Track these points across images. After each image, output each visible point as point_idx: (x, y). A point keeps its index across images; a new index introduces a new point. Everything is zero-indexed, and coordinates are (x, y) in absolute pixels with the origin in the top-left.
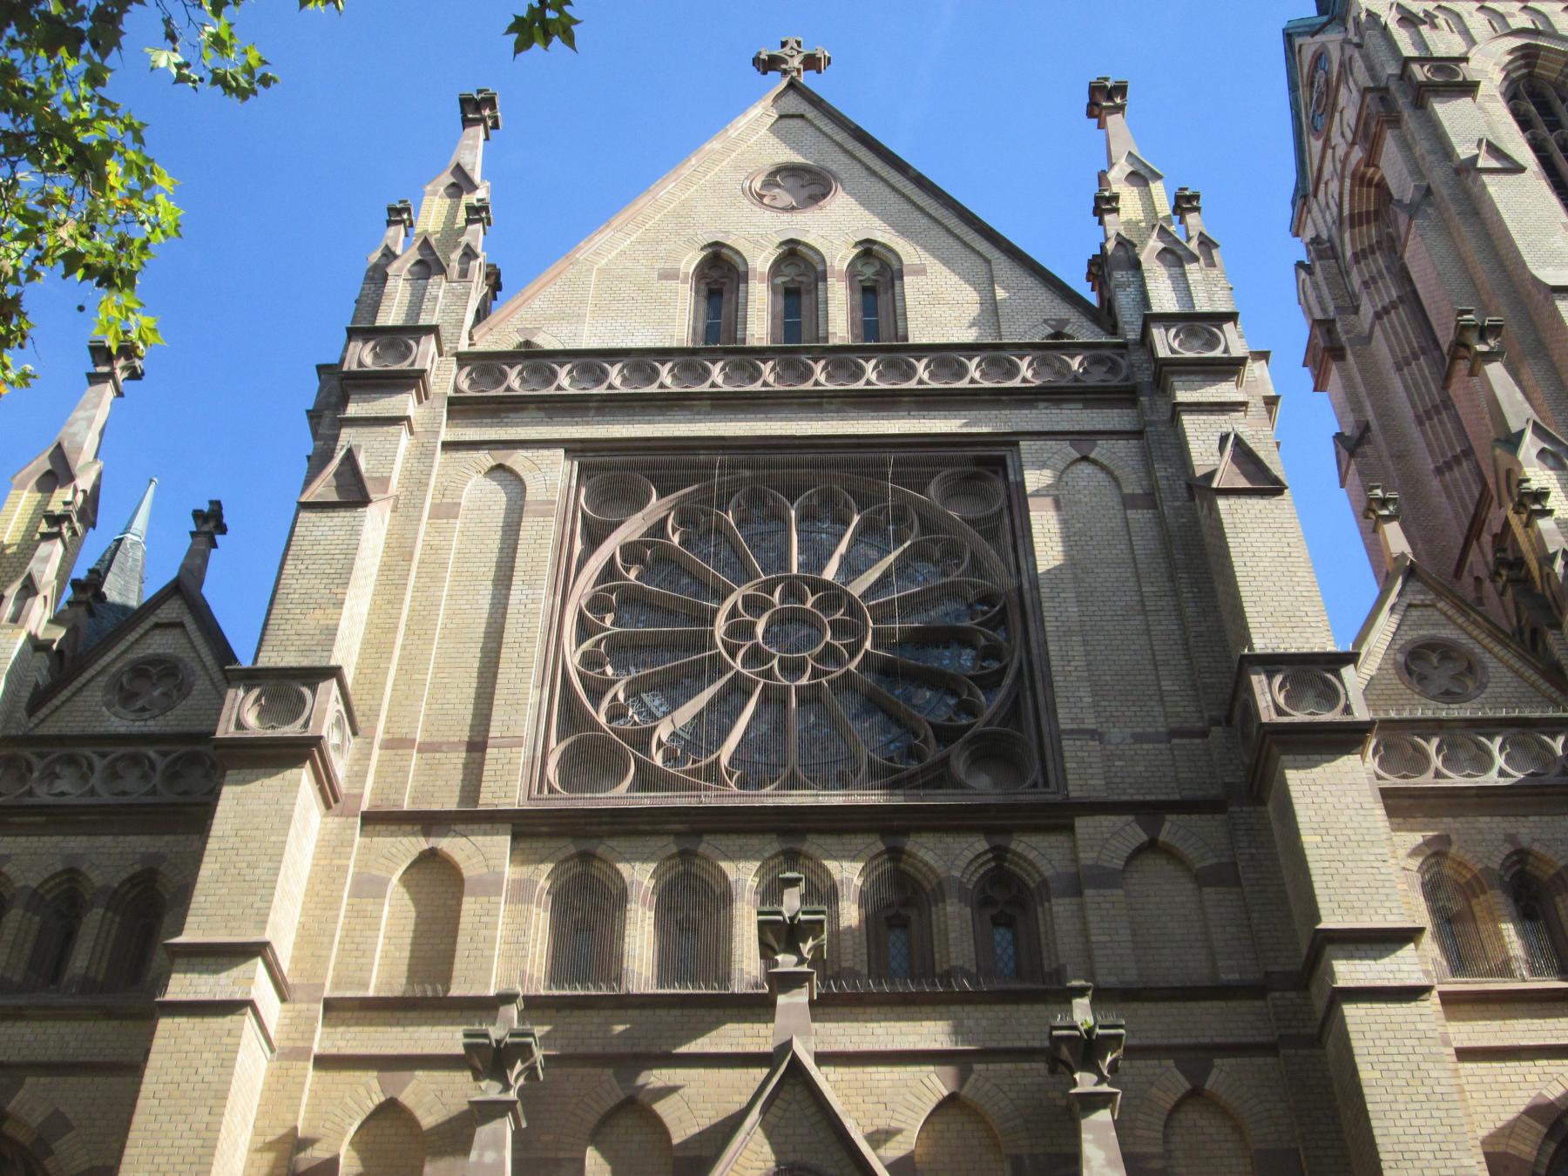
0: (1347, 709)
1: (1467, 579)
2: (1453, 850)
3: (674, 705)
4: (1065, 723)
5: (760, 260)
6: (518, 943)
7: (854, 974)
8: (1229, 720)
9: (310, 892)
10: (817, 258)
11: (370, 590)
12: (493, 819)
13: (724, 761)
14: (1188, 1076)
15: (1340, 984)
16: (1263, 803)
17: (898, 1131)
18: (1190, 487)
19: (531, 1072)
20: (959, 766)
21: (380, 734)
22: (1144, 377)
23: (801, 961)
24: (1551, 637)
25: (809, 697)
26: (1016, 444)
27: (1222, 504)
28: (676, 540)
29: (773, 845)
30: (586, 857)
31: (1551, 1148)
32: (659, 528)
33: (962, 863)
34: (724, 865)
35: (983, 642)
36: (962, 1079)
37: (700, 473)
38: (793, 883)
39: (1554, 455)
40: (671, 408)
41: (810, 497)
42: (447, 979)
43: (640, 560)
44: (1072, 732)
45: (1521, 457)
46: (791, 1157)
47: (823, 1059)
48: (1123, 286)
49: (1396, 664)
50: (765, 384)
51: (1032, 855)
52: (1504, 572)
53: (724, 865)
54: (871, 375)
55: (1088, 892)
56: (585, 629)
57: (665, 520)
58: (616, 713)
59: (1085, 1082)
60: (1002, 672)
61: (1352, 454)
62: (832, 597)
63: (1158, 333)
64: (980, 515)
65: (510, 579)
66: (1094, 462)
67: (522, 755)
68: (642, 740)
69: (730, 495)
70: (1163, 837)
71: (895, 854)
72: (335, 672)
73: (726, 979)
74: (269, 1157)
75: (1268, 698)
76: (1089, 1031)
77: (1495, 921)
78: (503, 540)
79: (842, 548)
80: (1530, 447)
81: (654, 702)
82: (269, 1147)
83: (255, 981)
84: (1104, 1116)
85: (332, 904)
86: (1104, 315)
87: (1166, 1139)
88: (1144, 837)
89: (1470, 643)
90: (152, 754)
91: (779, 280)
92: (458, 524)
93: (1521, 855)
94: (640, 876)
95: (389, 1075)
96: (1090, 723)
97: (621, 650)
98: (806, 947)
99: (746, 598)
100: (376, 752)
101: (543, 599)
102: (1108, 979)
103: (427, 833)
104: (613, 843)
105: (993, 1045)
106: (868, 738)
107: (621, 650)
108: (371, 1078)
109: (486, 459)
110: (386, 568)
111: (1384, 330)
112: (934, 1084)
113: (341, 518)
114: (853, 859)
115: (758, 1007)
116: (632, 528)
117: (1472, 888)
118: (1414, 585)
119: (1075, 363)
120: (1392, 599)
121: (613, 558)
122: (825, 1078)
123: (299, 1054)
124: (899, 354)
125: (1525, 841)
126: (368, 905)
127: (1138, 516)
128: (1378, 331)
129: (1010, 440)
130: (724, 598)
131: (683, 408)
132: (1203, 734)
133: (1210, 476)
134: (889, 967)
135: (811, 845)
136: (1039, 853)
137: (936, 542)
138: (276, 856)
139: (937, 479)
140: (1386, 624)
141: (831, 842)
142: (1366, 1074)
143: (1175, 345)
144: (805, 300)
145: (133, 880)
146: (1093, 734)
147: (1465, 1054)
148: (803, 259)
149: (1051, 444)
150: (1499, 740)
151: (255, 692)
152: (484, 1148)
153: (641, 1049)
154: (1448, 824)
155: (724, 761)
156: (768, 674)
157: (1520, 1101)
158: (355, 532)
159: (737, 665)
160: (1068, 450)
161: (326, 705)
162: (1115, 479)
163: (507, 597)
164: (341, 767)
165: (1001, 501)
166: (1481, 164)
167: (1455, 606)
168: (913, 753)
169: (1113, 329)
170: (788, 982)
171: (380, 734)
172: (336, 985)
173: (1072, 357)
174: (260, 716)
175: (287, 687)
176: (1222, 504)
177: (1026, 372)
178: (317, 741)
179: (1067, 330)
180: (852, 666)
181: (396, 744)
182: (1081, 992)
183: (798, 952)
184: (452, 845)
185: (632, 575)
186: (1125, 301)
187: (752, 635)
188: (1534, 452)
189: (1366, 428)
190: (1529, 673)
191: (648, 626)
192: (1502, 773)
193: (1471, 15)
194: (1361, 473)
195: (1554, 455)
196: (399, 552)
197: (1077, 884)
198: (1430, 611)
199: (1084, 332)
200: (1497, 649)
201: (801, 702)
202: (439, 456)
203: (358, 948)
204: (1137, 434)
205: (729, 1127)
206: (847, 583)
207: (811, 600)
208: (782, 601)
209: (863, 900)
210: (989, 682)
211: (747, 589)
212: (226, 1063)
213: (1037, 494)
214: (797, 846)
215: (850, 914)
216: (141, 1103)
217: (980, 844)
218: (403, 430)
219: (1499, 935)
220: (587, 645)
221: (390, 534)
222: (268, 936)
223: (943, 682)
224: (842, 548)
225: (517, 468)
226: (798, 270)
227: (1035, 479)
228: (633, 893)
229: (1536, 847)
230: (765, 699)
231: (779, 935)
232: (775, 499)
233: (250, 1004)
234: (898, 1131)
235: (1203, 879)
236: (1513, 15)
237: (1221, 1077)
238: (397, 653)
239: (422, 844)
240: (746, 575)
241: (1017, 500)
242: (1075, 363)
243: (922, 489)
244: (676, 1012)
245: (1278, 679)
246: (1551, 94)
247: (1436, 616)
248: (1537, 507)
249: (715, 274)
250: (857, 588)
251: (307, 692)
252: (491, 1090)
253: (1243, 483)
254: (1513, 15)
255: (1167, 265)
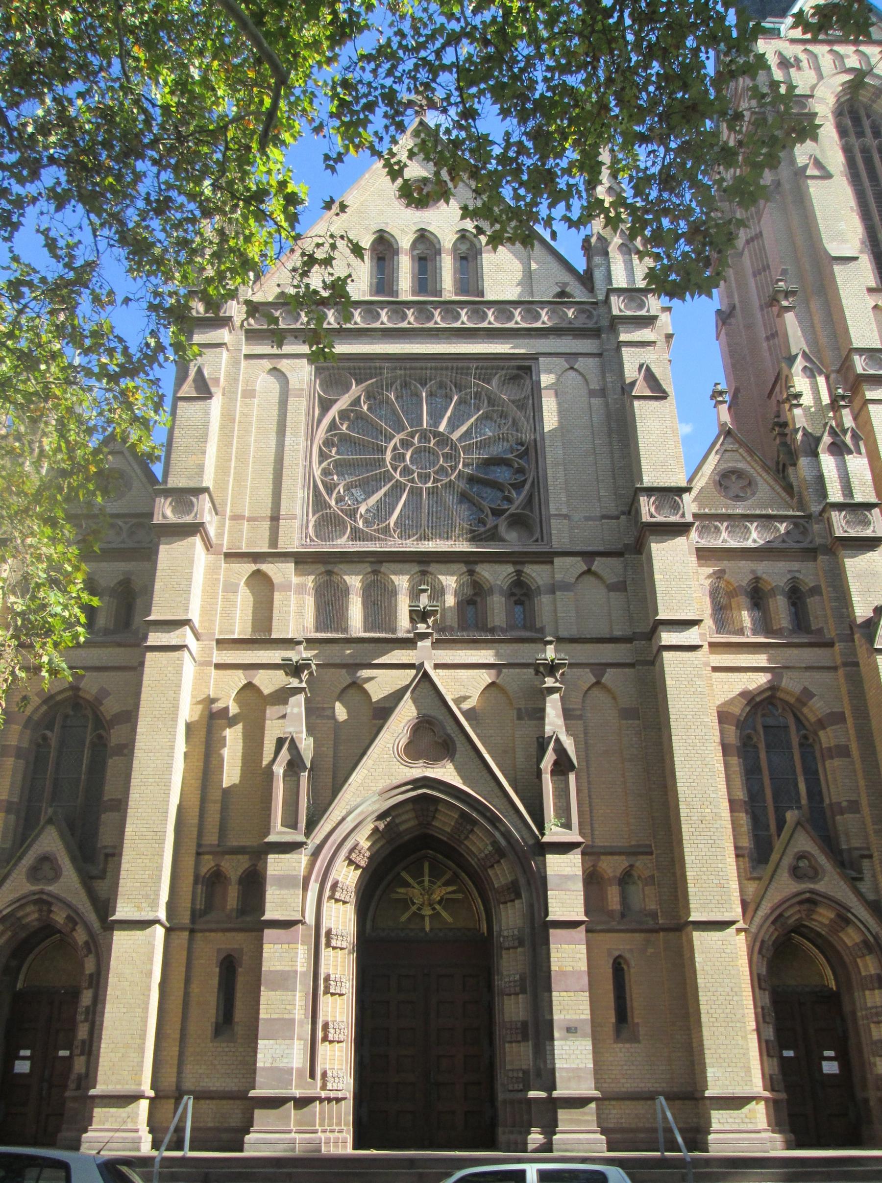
0: (683, 515)
1: (774, 400)
2: (726, 577)
3: (368, 495)
4: (553, 511)
5: (405, 242)
6: (300, 614)
7: (452, 629)
8: (629, 513)
9: (204, 591)
10: (435, 241)
11: (216, 440)
12: (284, 556)
13: (392, 525)
14: (595, 676)
15: (663, 643)
16: (641, 554)
17: (469, 697)
18: (623, 388)
19: (311, 674)
20: (502, 529)
21: (228, 513)
22: (605, 323)
23: (428, 627)
24: (790, 470)
25: (431, 492)
26: (537, 359)
27: (636, 403)
28: (365, 408)
29: (416, 568)
30: (329, 573)
31: (748, 709)
32: (356, 402)
33: (501, 578)
34: (393, 577)
35: (516, 465)
36: (498, 675)
37: (376, 372)
38: (425, 591)
39: (811, 370)
40: (360, 336)
41: (432, 386)
42: (270, 630)
43: (348, 418)
44: (556, 515)
45: (793, 371)
46: (423, 712)
47: (437, 666)
48: (598, 266)
49: (714, 481)
50: (409, 323)
51: (534, 575)
52: (777, 429)
53: (393, 577)
54: (464, 320)
55: (558, 593)
56: (323, 456)
57: (360, 396)
58: (339, 500)
59: (549, 682)
60: (525, 481)
61: (724, 323)
62: (443, 440)
63: (613, 299)
64: (518, 398)
65: (284, 431)
66: (576, 370)
67: (297, 523)
68: (352, 514)
69: (392, 383)
70: (593, 568)
71: (471, 573)
72: (206, 490)
73: (394, 631)
74: (200, 707)
75: (648, 509)
76: (552, 661)
77: (740, 610)
78: (279, 410)
79: (449, 414)
80: (799, 364)
81: (358, 493)
82: (199, 703)
83: (185, 635)
84: (556, 696)
85: (214, 596)
86: (587, 279)
87: (583, 701)
88: (585, 568)
89: (752, 471)
90: (120, 523)
91: (416, 252)
92: (256, 401)
93: (757, 579)
94: (354, 582)
95: (247, 672)
96: (564, 511)
97: (341, 467)
98: (430, 621)
99: (401, 440)
100: (227, 522)
101: (302, 442)
102: (563, 633)
103: (255, 562)
104: (341, 566)
105: (511, 661)
106: (461, 515)
107: (341, 467)
108: (240, 673)
109: (267, 364)
110: (223, 427)
111: (749, 251)
112: (486, 677)
113: (199, 405)
114: (452, 575)
115: (409, 643)
116: (343, 402)
117: (732, 594)
118: (729, 440)
119: (570, 313)
120: (717, 447)
121: (334, 418)
122: (437, 677)
123: (208, 663)
124: (478, 307)
125: (759, 574)
126: (231, 595)
127: (596, 401)
128: (746, 252)
129: (534, 357)
130: (391, 439)
131: (366, 336)
132: (618, 518)
133: (633, 384)
134: (469, 623)
135: (433, 568)
136: (536, 574)
137: (495, 411)
138: (189, 579)
139: (496, 378)
140: (713, 459)
141: (442, 567)
142: (669, 682)
143: (622, 307)
144: (430, 265)
145: (120, 583)
146: (566, 516)
147: (716, 669)
148: (428, 239)
149: (555, 359)
150: (755, 524)
151: (169, 500)
152: (293, 707)
153: (358, 661)
154: (725, 564)
155: (392, 525)
156: (412, 481)
157: (738, 690)
158: (207, 413)
159: (397, 476)
160: (562, 363)
161: (204, 503)
162: (586, 380)
163: (284, 441)
164: (212, 531)
165: (528, 391)
166: (809, 172)
167: (747, 451)
168: (482, 522)
169: (591, 290)
170: (423, 636)
171: (228, 513)
172: (221, 633)
173: (569, 309)
174: (173, 511)
175: (185, 496)
176: (636, 403)
177: (545, 319)
178: (202, 524)
179: (568, 289)
180: (453, 477)
181: (236, 517)
182: (550, 643)
183: (426, 623)
184: (267, 568)
185: (344, 427)
186: (598, 275)
187: (404, 460)
188: (800, 368)
189: (733, 308)
190: (777, 488)
191: (353, 453)
192: (754, 541)
193: (823, 56)
194: (727, 335)
195: (811, 370)
196: (228, 418)
197: (552, 590)
198: (734, 454)
199: (579, 294)
200: (764, 475)
201: (428, 494)
202: (243, 363)
203: (228, 615)
204: (600, 355)
205: (397, 697)
206: (451, 432)
207: (433, 441)
208: (419, 442)
209: (456, 594)
210: (518, 486)
211: (402, 436)
212: (179, 672)
213: (546, 388)
214: (426, 569)
215: (450, 600)
216: (143, 689)
217: (510, 569)
218: (224, 350)
219: (741, 616)
220: (324, 465)
221: (223, 408)
222: (190, 617)
223: (494, 485)
224: (449, 414)
225: (283, 370)
226: (426, 246)
227: (546, 379)
228: (351, 590)
229: (764, 576)
230: (411, 492)
231: (419, 615)
232: (415, 386)
233: (186, 646)
234: (469, 697)
235: (612, 588)
236: (848, 56)
237: (610, 677)
238: (232, 471)
239: (253, 567)
240: (402, 428)
241: (536, 392)
242: (570, 313)
243: (488, 382)
244: (373, 645)
245: (653, 499)
246: (862, 113)
247: (738, 456)
248: (795, 402)
249: (381, 248)
250: (455, 436)
251: (194, 499)
252: (295, 683)
253: (648, 393)
254: (848, 56)
255: (623, 254)
